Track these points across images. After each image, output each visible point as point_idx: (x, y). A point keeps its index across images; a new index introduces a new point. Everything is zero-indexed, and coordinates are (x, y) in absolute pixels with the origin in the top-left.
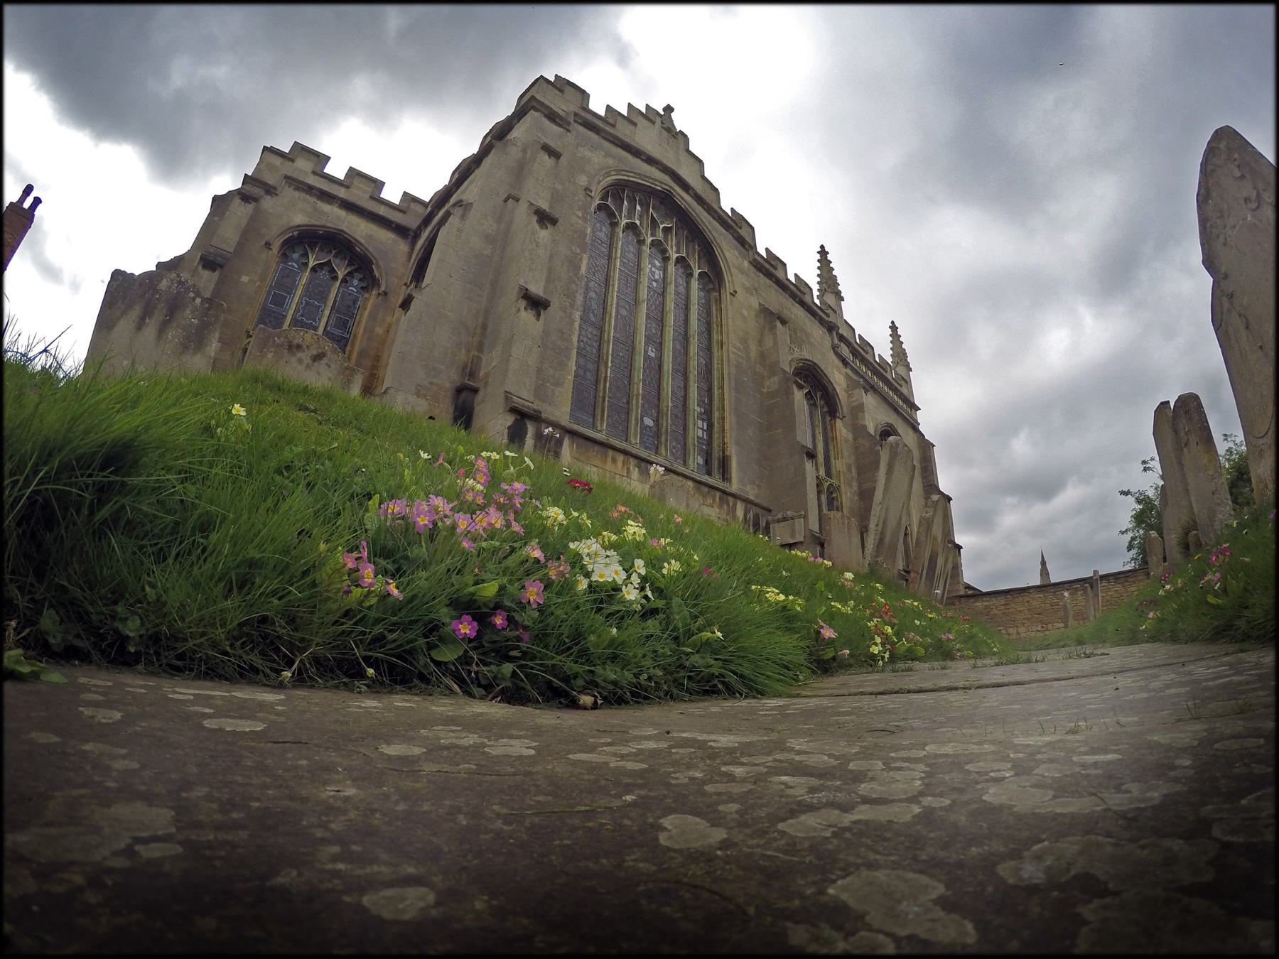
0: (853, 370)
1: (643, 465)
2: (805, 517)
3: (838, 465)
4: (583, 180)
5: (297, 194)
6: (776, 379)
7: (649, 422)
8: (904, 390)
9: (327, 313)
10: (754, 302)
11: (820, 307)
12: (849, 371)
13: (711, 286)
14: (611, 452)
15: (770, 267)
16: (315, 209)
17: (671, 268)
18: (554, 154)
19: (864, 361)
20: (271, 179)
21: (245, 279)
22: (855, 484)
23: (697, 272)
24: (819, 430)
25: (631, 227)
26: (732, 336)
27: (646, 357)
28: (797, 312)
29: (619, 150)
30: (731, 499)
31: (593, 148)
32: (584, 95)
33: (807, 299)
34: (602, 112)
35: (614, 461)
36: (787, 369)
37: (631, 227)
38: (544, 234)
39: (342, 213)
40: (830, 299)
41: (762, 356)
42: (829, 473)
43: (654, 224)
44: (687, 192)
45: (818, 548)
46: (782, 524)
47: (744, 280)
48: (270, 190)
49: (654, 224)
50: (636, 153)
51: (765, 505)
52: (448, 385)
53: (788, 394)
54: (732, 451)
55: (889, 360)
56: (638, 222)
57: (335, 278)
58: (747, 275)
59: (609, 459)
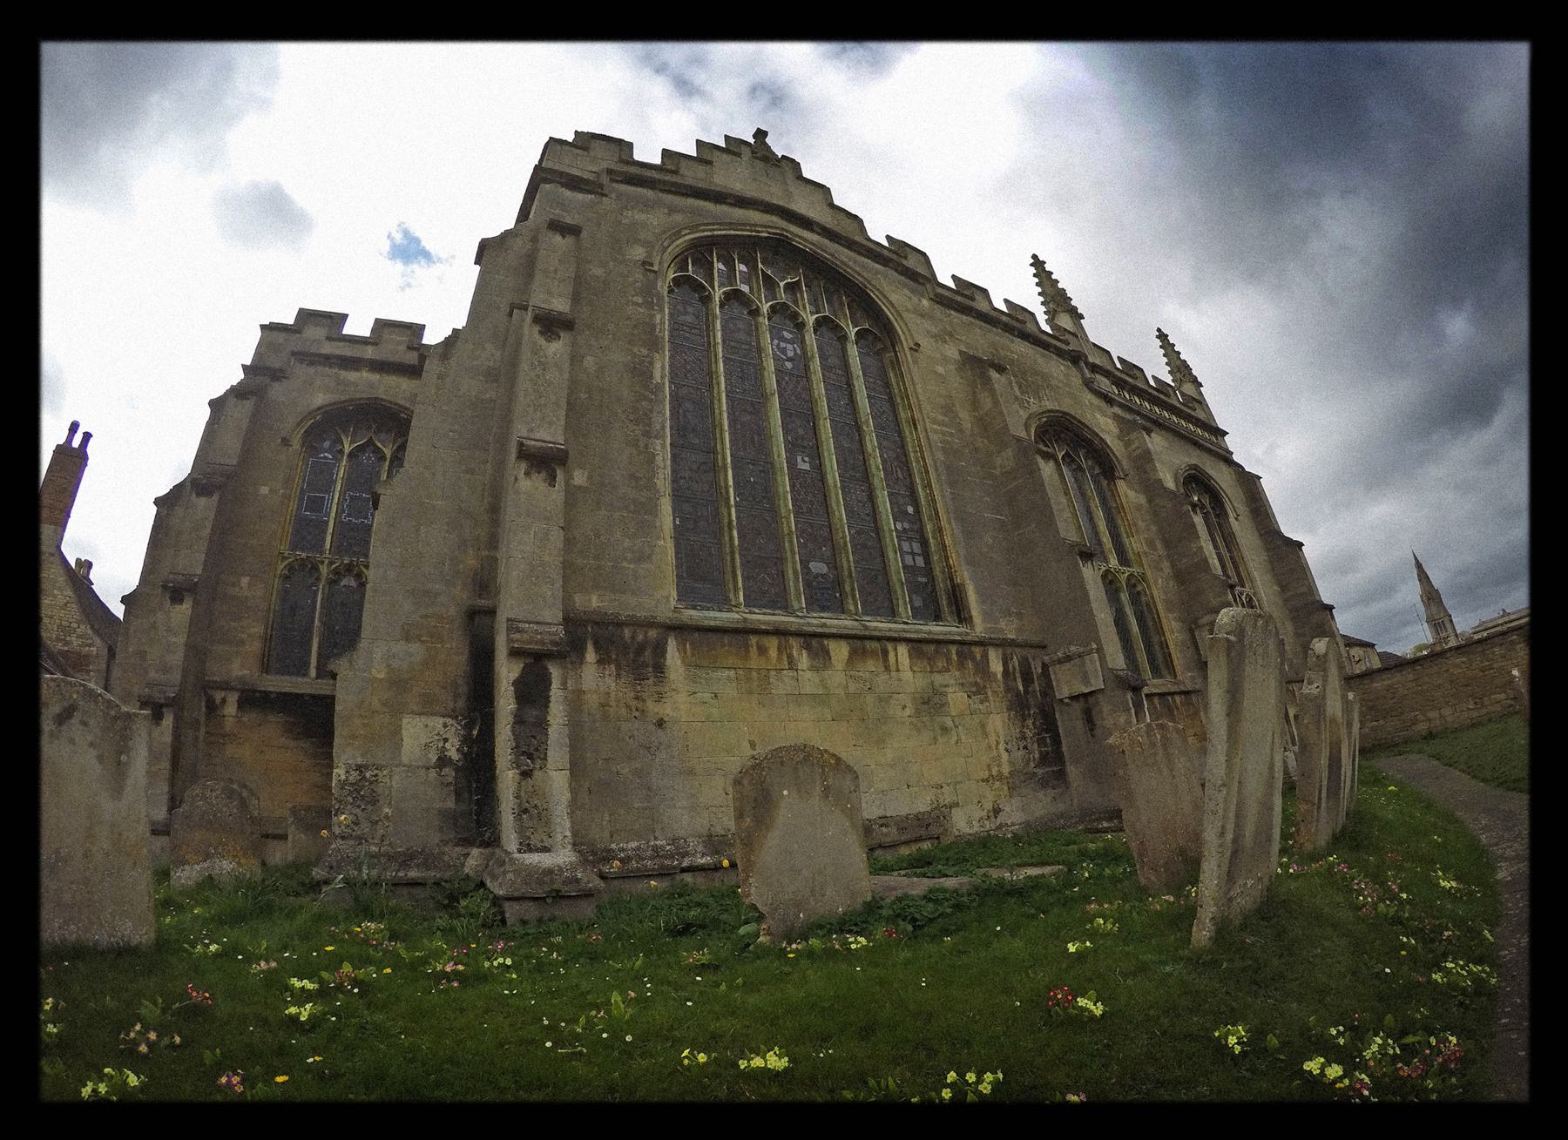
0: (1121, 406)
1: (814, 642)
2: (1100, 650)
3: (1134, 544)
4: (638, 253)
5: (311, 370)
6: (1010, 452)
7: (818, 567)
8: (1201, 415)
10: (952, 352)
11: (1056, 333)
12: (1117, 410)
13: (880, 346)
14: (753, 640)
15: (966, 299)
17: (810, 338)
18: (572, 231)
19: (1135, 390)
20: (275, 362)
22: (1166, 565)
23: (852, 332)
24: (1096, 502)
25: (734, 296)
26: (927, 408)
27: (795, 473)
28: (1021, 348)
29: (690, 201)
30: (977, 651)
31: (648, 206)
32: (625, 147)
33: (1030, 327)
34: (657, 160)
35: (762, 651)
36: (1023, 434)
37: (734, 296)
38: (557, 348)
39: (375, 377)
40: (1065, 321)
41: (983, 424)
42: (1124, 560)
43: (770, 283)
44: (812, 231)
45: (1129, 695)
46: (1067, 666)
47: (927, 325)
48: (277, 375)
49: (770, 283)
50: (719, 197)
51: (1035, 639)
52: (452, 611)
53: (1034, 471)
54: (965, 576)
55: (1168, 379)
56: (745, 288)
57: (383, 458)
58: (932, 318)
59: (754, 650)
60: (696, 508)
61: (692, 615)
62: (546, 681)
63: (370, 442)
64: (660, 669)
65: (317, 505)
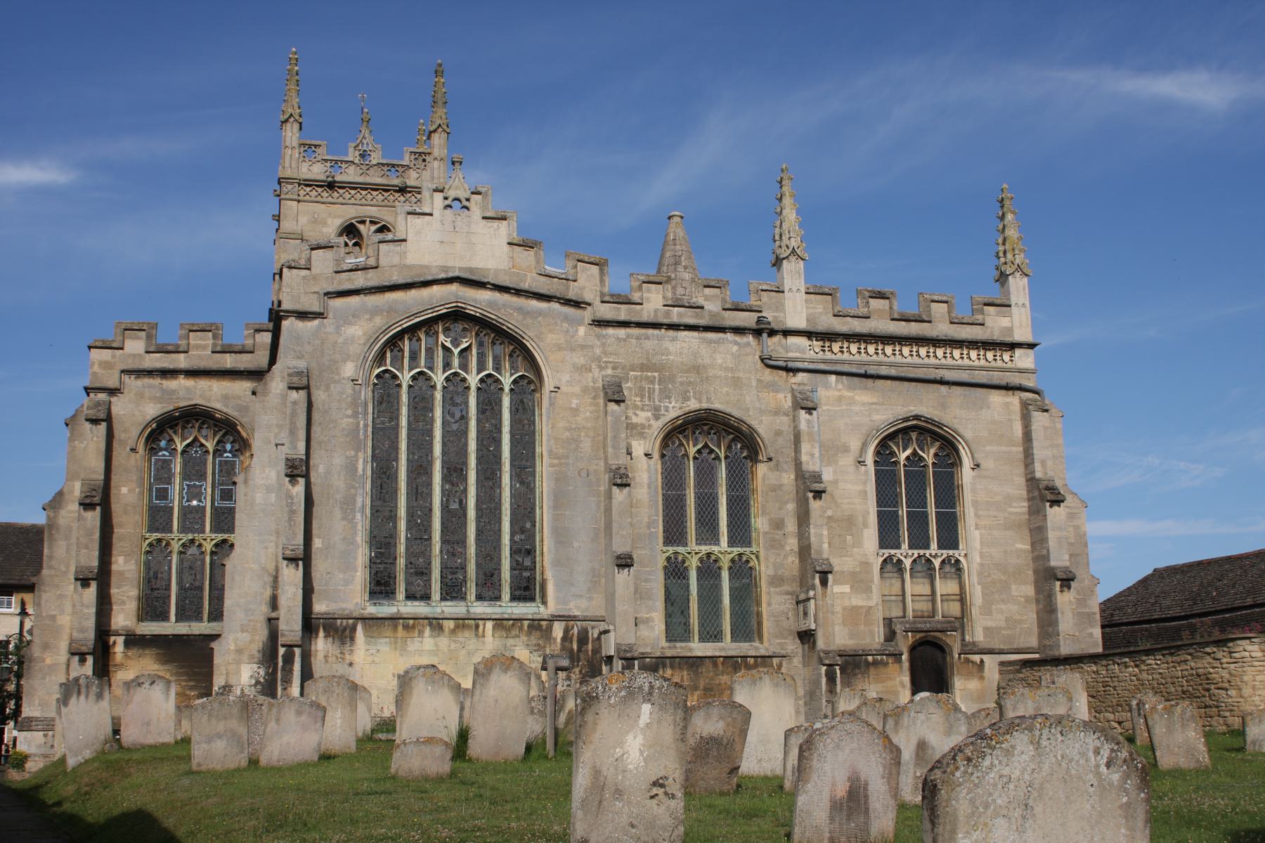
9: (209, 490)
16: (163, 391)
21: (124, 490)
57: (207, 452)
60: (382, 546)
61: (372, 610)
62: (293, 654)
63: (196, 439)
64: (352, 639)
65: (163, 494)
